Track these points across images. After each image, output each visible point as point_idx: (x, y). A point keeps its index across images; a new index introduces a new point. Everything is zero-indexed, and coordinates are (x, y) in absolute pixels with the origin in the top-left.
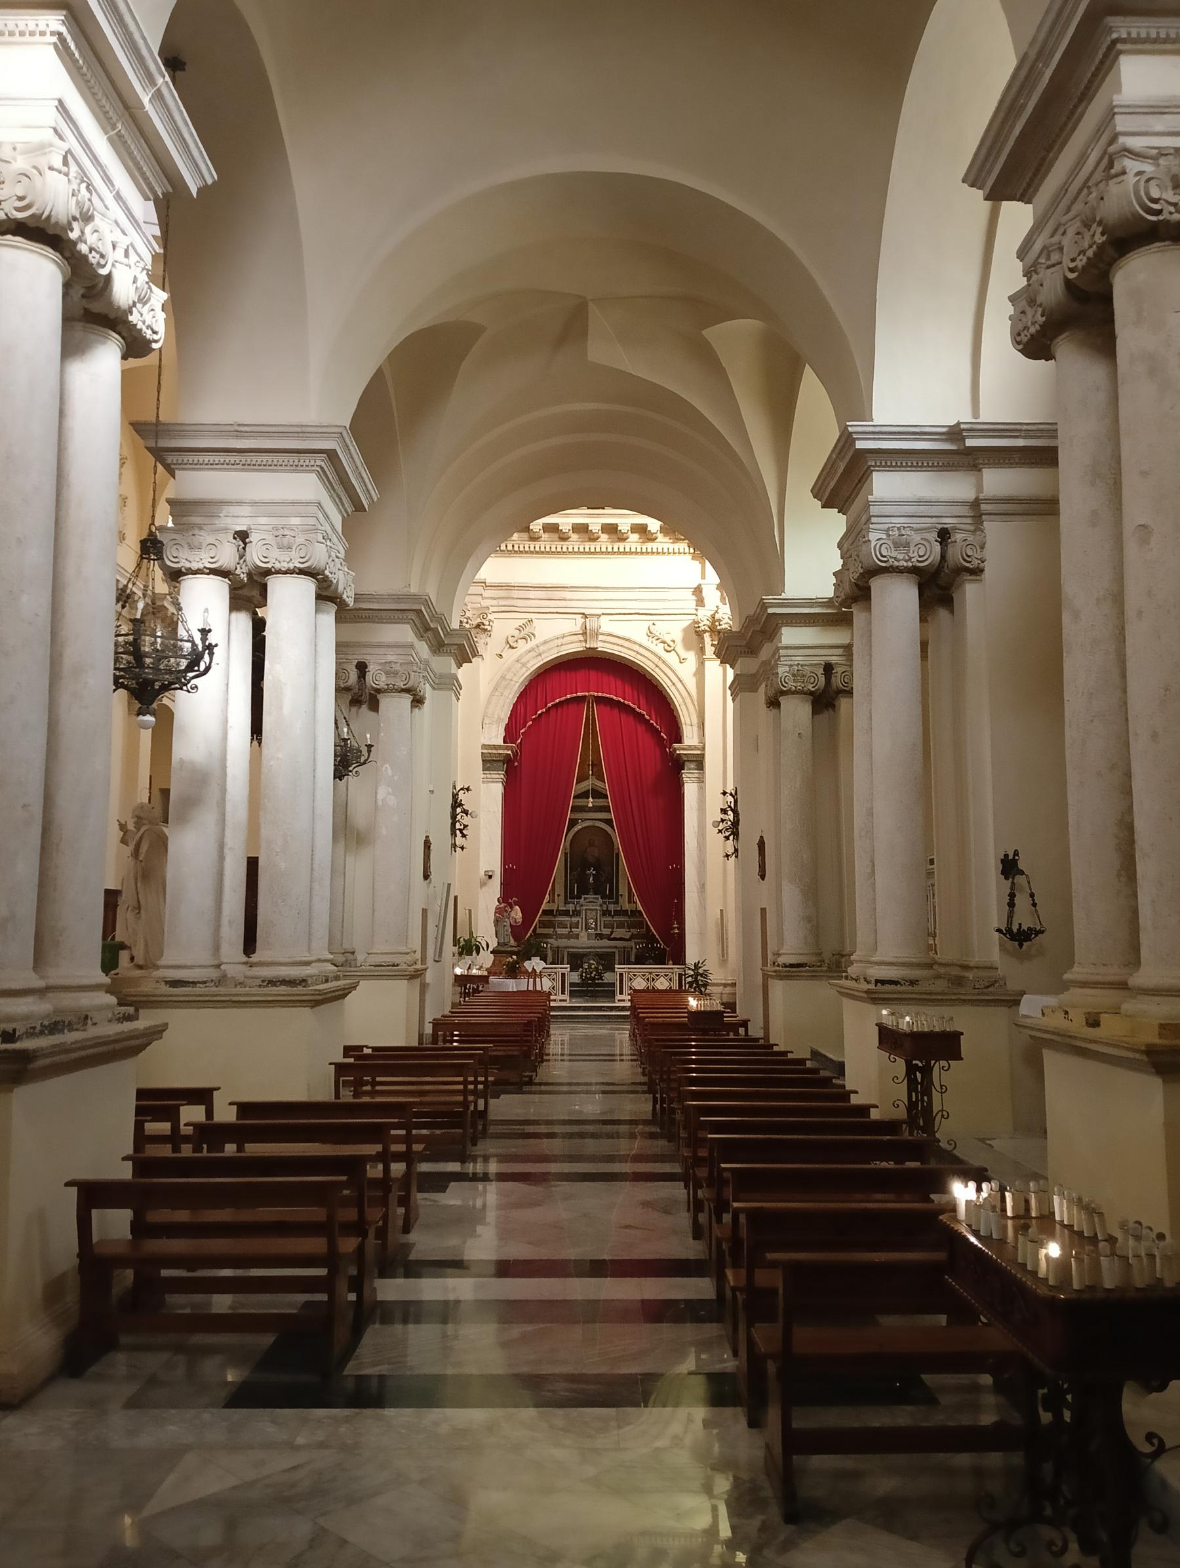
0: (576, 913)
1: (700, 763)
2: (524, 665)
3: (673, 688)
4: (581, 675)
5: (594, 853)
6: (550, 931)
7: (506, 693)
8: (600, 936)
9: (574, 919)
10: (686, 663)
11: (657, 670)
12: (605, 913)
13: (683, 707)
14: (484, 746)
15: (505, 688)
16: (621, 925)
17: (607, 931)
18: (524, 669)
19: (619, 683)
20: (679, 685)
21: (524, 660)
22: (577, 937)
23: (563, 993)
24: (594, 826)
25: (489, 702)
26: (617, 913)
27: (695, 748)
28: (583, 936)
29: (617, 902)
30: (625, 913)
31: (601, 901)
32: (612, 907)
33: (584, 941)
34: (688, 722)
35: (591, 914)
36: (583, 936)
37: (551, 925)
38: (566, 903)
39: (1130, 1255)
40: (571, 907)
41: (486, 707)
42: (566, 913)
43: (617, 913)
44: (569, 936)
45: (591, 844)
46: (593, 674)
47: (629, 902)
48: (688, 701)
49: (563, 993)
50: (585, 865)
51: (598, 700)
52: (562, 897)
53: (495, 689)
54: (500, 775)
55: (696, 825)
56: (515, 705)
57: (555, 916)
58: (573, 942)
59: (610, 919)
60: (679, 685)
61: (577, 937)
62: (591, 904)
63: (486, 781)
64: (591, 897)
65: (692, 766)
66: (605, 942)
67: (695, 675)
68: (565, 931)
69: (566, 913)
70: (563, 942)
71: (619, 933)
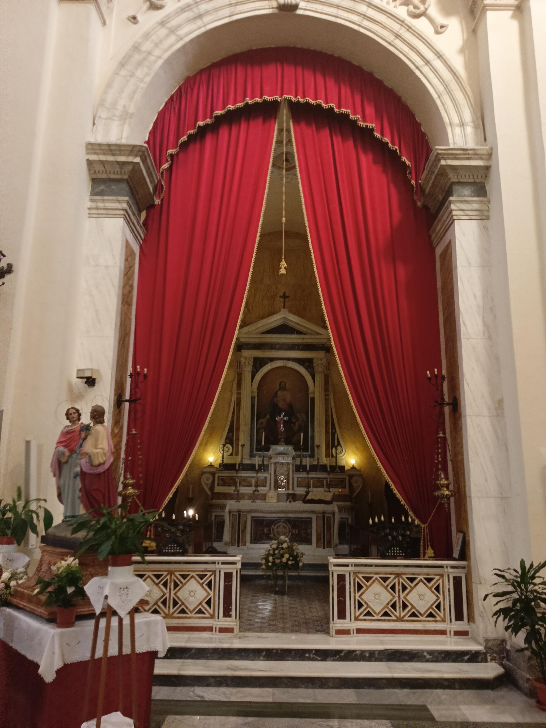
0: (263, 468)
1: (480, 181)
2: (172, 31)
3: (426, 69)
4: (271, 71)
5: (285, 398)
6: (231, 490)
7: (140, 73)
8: (293, 497)
9: (262, 475)
10: (447, 33)
11: (398, 43)
12: (299, 468)
13: (446, 98)
14: (92, 147)
15: (140, 64)
16: (319, 483)
17: (301, 491)
18: (173, 38)
19: (331, 84)
20: (438, 64)
21: (173, 23)
22: (264, 497)
23: (227, 613)
24: (285, 367)
25: (109, 85)
26: (314, 468)
27: (476, 155)
28: (272, 496)
29: (312, 456)
30: (324, 468)
31: (294, 453)
32: (307, 462)
33: (272, 504)
34: (456, 120)
35: (281, 470)
36: (272, 496)
37: (232, 482)
38: (252, 456)
39: (287, 492)
40: (257, 461)
41: (105, 92)
42: (251, 468)
43: (314, 468)
44: (254, 497)
45: (282, 388)
46: (289, 71)
47: (327, 455)
48: (454, 86)
49: (227, 613)
50: (275, 410)
51: (300, 112)
52: (247, 449)
53: (122, 65)
54: (121, 202)
55: (479, 294)
56: (162, 115)
57: (238, 471)
58: (259, 504)
59: (304, 475)
60: (438, 64)
61: (264, 497)
62: (282, 455)
63: (95, 213)
64: (281, 448)
65: (467, 191)
66: (299, 505)
67: (462, 51)
68: (248, 490)
69: (251, 468)
70: (245, 505)
71: (317, 493)
